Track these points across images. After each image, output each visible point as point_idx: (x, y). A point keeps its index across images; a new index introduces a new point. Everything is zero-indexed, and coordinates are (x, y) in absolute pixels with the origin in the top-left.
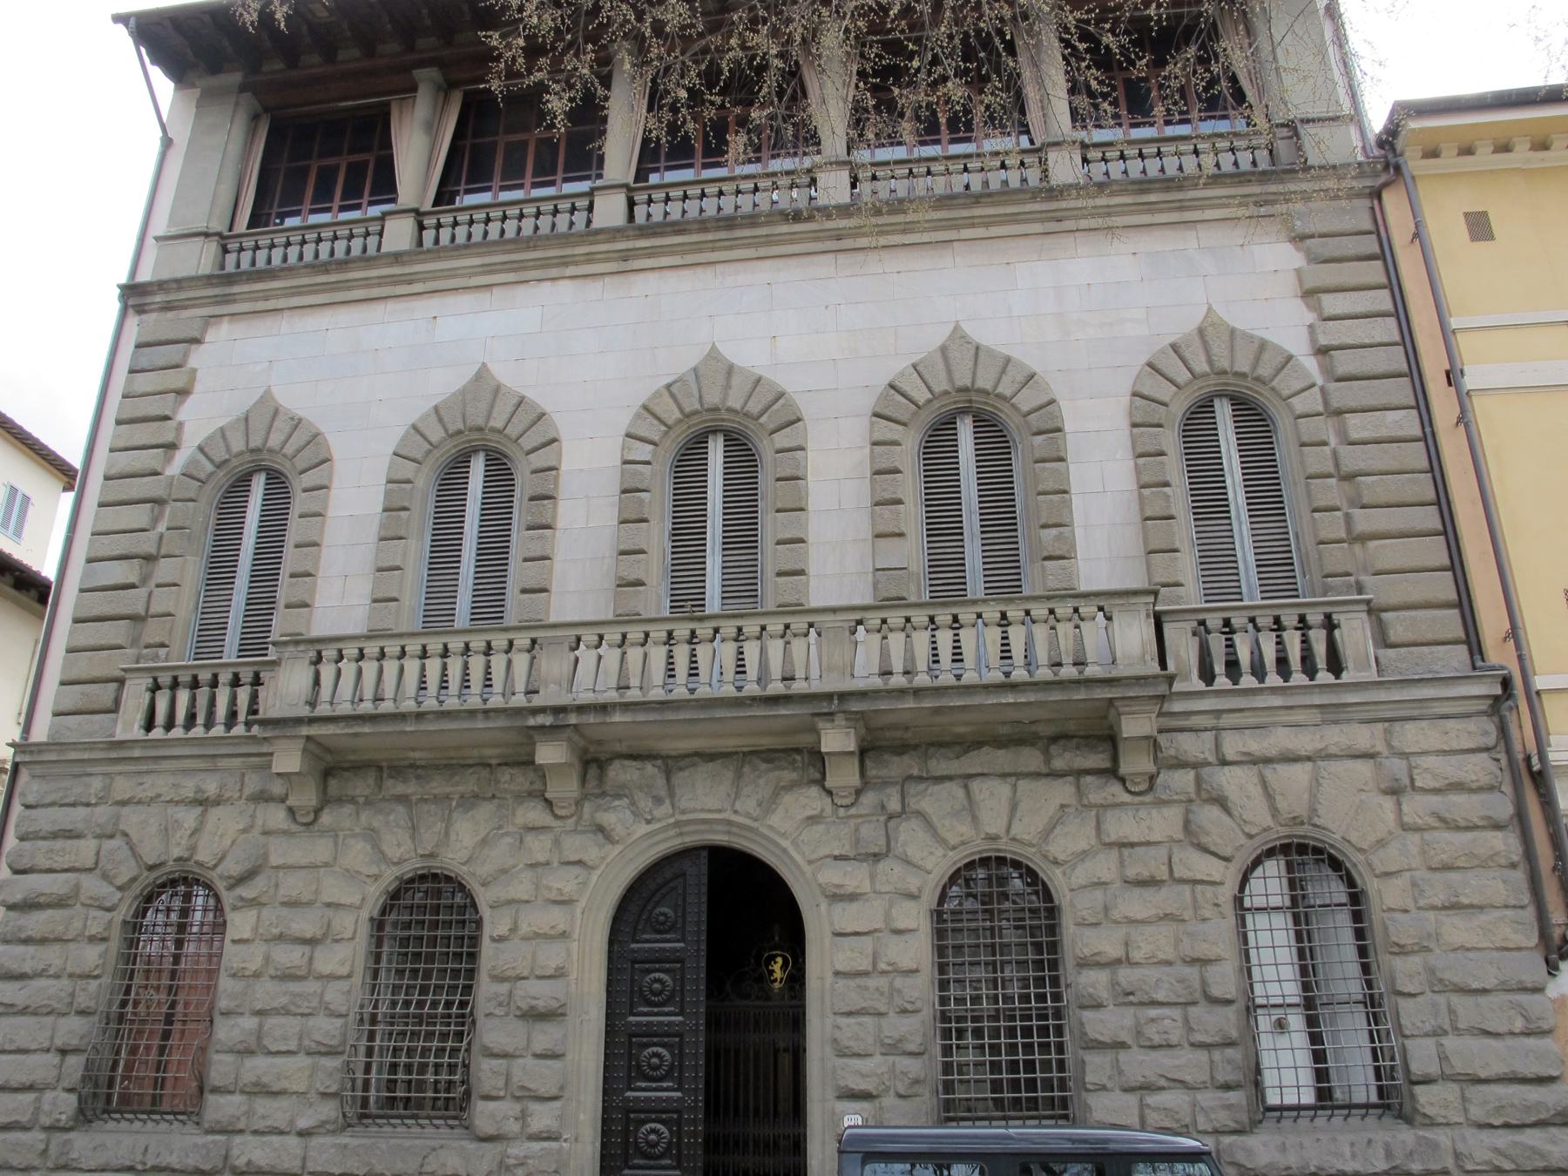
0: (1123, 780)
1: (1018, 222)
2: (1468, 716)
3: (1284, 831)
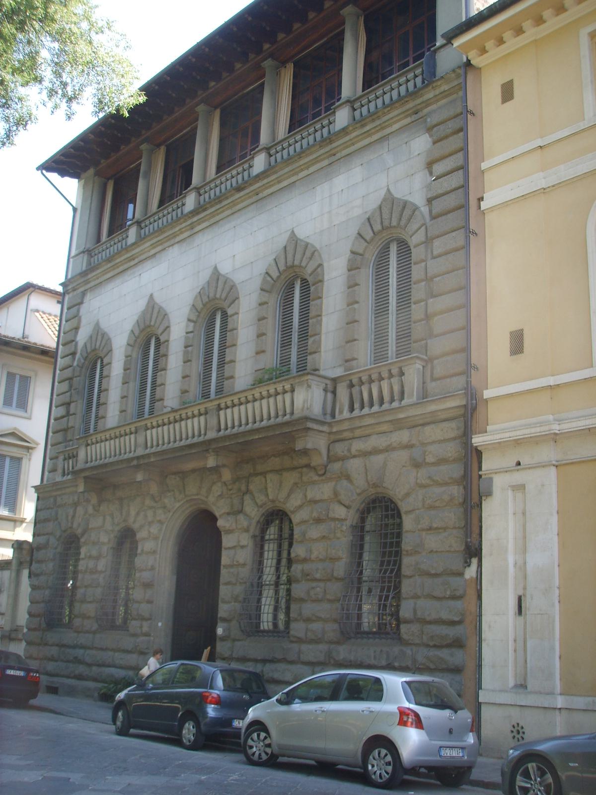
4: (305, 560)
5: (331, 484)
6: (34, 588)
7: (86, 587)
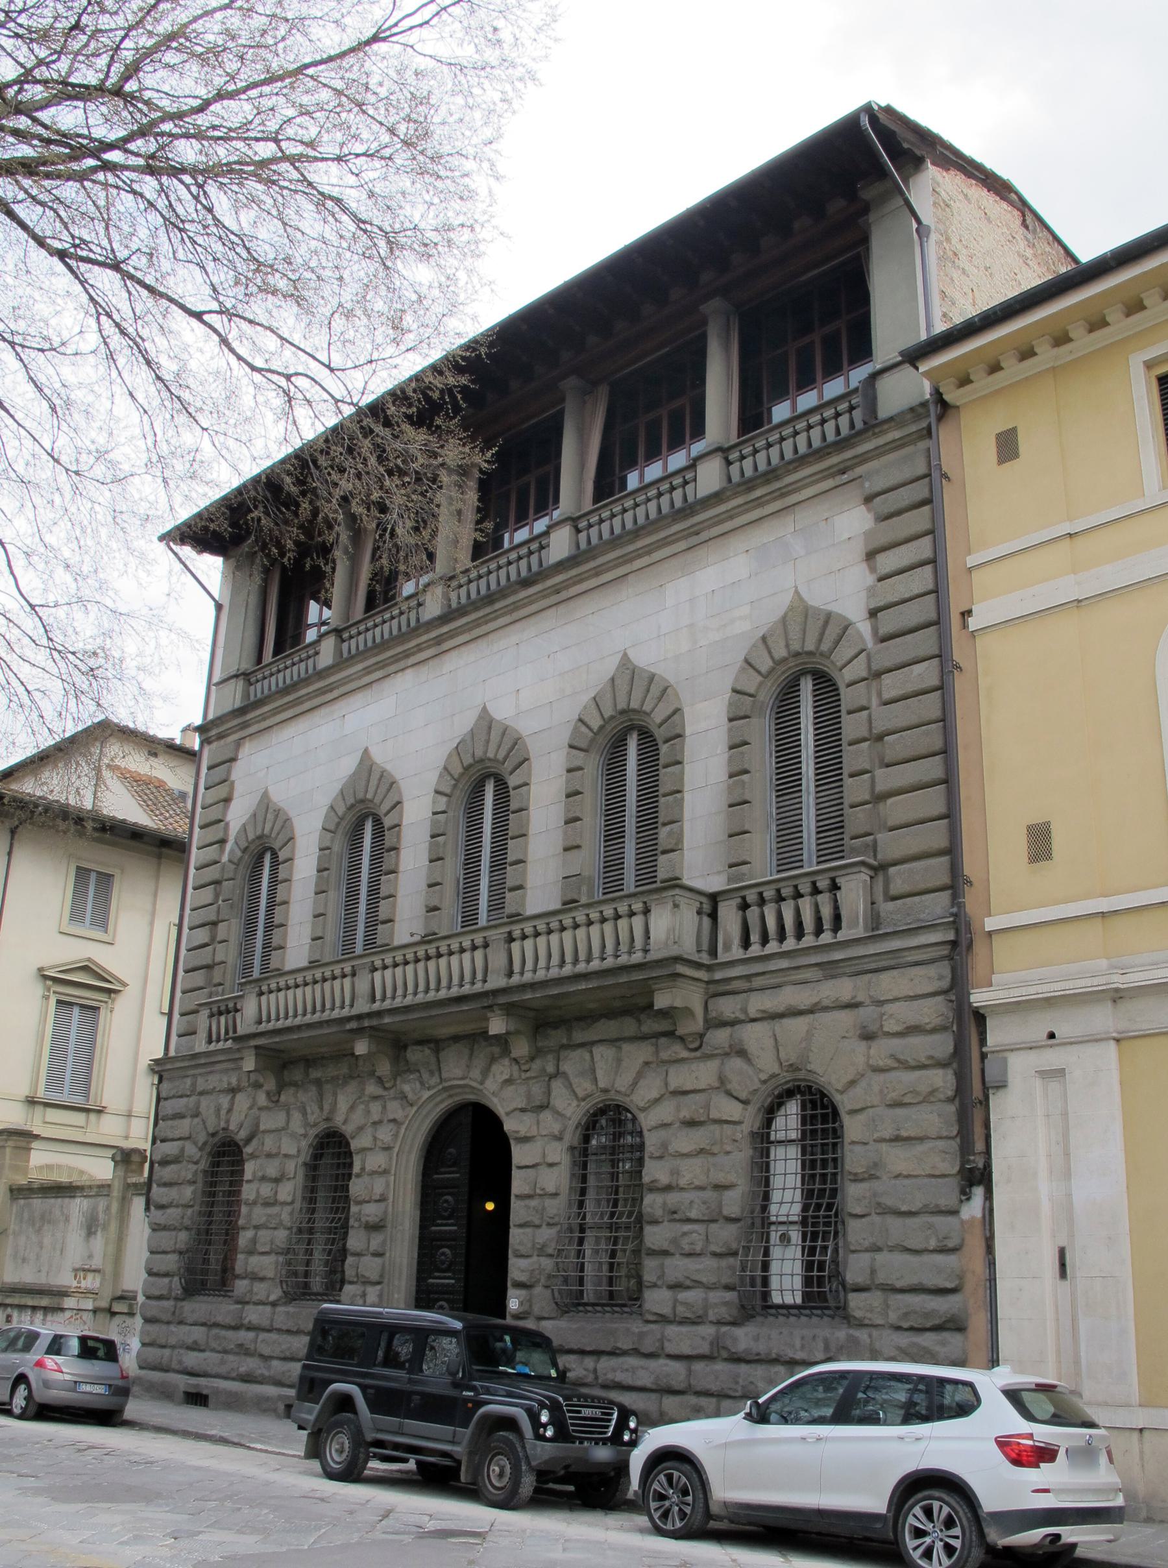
0: (682, 1039)
1: (669, 544)
2: (932, 961)
3: (789, 1076)
4: (668, 1188)
5: (713, 1065)
6: (156, 1228)
7: (256, 1227)
